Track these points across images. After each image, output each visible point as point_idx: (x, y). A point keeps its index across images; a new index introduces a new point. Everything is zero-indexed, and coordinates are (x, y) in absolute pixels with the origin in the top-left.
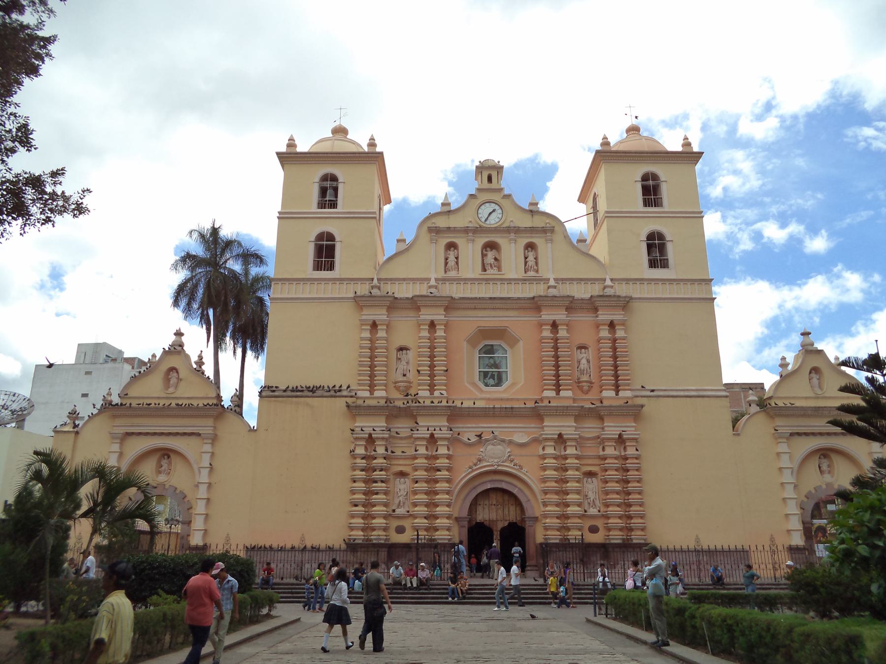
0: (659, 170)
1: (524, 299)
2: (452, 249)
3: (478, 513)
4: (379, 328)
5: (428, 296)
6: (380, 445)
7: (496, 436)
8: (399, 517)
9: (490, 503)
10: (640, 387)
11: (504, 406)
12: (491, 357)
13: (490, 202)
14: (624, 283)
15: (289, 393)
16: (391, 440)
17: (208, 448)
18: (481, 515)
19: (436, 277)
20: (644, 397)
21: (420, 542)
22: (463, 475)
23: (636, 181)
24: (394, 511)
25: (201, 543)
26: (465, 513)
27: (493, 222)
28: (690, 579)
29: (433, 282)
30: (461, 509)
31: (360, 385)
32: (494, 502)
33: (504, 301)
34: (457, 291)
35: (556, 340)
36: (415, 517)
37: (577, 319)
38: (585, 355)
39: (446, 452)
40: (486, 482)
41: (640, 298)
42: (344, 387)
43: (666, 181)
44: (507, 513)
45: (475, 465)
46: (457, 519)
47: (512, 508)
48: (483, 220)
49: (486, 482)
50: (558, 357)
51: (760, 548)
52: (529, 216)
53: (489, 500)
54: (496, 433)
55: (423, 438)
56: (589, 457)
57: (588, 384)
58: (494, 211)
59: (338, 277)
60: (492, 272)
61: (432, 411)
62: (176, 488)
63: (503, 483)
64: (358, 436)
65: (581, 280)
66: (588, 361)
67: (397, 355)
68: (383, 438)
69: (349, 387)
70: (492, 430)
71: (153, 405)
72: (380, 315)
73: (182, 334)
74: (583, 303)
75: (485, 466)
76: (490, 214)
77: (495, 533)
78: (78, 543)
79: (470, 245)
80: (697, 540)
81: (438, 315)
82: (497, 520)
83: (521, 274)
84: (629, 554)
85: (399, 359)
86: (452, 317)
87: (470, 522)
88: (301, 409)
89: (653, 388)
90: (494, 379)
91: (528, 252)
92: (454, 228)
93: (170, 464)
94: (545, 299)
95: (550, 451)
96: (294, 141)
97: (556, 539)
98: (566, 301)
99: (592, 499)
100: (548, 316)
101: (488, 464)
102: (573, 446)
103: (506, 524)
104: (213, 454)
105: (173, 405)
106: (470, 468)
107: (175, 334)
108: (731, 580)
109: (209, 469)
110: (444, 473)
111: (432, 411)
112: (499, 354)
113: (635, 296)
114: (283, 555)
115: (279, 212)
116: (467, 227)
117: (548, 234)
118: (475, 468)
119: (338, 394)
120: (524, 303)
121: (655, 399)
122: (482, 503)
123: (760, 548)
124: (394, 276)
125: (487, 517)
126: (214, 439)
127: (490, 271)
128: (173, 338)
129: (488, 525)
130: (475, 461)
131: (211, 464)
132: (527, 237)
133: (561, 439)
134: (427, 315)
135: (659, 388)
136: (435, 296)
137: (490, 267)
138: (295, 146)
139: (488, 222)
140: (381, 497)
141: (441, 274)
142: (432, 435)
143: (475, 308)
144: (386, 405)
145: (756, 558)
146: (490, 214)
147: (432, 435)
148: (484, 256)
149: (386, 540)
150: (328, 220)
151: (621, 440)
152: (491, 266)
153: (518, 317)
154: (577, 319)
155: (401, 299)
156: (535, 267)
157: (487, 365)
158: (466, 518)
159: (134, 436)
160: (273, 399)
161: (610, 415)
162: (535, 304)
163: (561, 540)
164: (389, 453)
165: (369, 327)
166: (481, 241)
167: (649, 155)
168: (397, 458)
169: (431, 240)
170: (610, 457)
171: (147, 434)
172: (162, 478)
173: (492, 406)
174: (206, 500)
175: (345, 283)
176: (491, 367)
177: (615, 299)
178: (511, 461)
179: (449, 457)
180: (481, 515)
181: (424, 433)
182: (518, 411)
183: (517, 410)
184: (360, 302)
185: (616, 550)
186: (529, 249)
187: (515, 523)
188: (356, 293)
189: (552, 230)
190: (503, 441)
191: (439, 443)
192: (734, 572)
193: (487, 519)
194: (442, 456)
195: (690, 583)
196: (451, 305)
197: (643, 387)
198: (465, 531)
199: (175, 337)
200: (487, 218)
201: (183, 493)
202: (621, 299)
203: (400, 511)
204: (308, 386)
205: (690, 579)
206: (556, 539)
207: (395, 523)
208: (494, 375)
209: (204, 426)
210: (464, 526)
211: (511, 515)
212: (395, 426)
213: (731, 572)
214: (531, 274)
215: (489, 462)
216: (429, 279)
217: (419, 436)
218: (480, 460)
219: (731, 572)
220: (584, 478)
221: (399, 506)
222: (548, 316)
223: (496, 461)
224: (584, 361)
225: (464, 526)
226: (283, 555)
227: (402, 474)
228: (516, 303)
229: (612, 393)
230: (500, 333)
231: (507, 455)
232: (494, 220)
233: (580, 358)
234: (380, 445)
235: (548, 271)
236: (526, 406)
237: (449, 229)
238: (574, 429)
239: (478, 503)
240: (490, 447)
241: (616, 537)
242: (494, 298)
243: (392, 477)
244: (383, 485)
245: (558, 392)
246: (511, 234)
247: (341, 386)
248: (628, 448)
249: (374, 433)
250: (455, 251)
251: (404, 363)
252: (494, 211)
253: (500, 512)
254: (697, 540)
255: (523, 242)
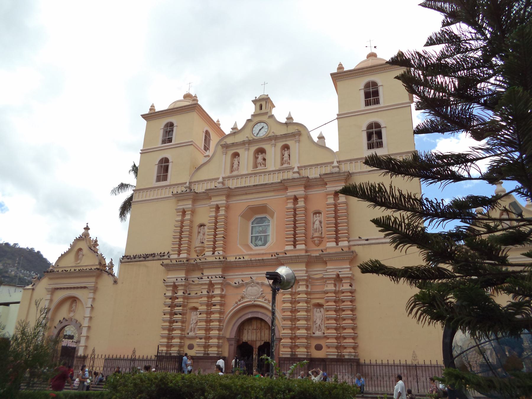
0: (376, 78)
1: (276, 183)
2: (237, 156)
3: (244, 335)
4: (220, 209)
5: (214, 189)
6: (217, 288)
7: (253, 280)
8: (318, 338)
9: (252, 328)
10: (358, 238)
11: (257, 259)
12: (260, 226)
13: (260, 122)
14: (348, 163)
15: (137, 259)
16: (189, 286)
17: (91, 295)
18: (246, 336)
19: (299, 165)
20: (360, 245)
21: (159, 354)
22: (231, 308)
23: (360, 90)
24: (188, 334)
25: (82, 355)
26: (233, 335)
27: (261, 135)
28: (388, 389)
29: (335, 164)
30: (230, 332)
31: (173, 251)
32: (255, 328)
33: (263, 187)
34: (233, 184)
35: (295, 210)
36: (327, 338)
37: (315, 192)
38: (318, 218)
39: (219, 292)
40: (248, 313)
41: (359, 172)
42: (166, 254)
43: (382, 85)
44: (263, 335)
45: (240, 301)
46: (229, 340)
47: (267, 332)
48: (255, 135)
49: (248, 313)
50: (217, 228)
51: (100, 357)
52: (285, 127)
53: (252, 326)
54: (254, 278)
55: (205, 284)
56: (318, 293)
57: (319, 239)
58: (263, 127)
59: (169, 184)
60: (260, 168)
61: (211, 265)
62: (77, 321)
63: (259, 313)
64: (167, 284)
65: (318, 165)
66: (320, 222)
67: (198, 230)
68: (182, 285)
69: (168, 253)
70: (250, 276)
71: (88, 270)
72: (188, 205)
73: (89, 229)
74: (316, 181)
75: (247, 301)
76: (260, 130)
77: (254, 350)
78: (93, 355)
79: (247, 152)
80: (415, 356)
81: (300, 192)
82: (256, 341)
83: (278, 167)
84: (341, 366)
85: (199, 232)
86: (232, 201)
87: (238, 341)
88: (140, 268)
89: (366, 238)
90: (261, 241)
91: (285, 151)
92: (236, 143)
93: (76, 306)
94: (288, 181)
95: (331, 287)
96: (197, 98)
97: (288, 354)
98: (303, 181)
99: (318, 324)
100: (291, 193)
101: (248, 300)
102: (303, 285)
103: (262, 343)
104: (94, 299)
105: (77, 270)
106: (236, 303)
107: (85, 229)
108: (374, 390)
109: (90, 308)
110: (302, 323)
111: (211, 265)
112: (265, 223)
113: (354, 171)
114: (141, 363)
115: (141, 150)
116: (244, 141)
117: (296, 137)
118: (239, 303)
119: (162, 258)
120: (275, 186)
121: (368, 246)
122: (247, 328)
123: (100, 357)
124: (198, 180)
125: (250, 338)
126: (95, 290)
127: (259, 167)
128: (83, 231)
129: (250, 344)
130: (239, 298)
131: (92, 306)
132: (283, 141)
133: (338, 279)
134: (215, 201)
135: (372, 238)
136: (218, 189)
137: (260, 165)
138: (343, 68)
139: (258, 136)
140: (179, 324)
141: (228, 174)
142: (211, 281)
143: (246, 194)
144: (224, 260)
145: (100, 362)
146: (260, 130)
147: (211, 281)
148: (256, 158)
149: (355, 356)
150: (166, 150)
151: (338, 279)
152: (261, 165)
153: (275, 196)
154: (315, 192)
155: (200, 193)
156: (289, 161)
157: (258, 232)
158: (233, 339)
159: (59, 290)
160: (127, 263)
161: (331, 260)
162: (283, 185)
163: (338, 355)
164: (187, 295)
165: (332, 196)
166: (253, 149)
167: (348, 73)
168: (192, 298)
169: (223, 152)
170: (331, 292)
171: (64, 288)
172: (72, 314)
173: (250, 259)
174: (87, 328)
175: (272, 174)
176: (260, 233)
177: (337, 175)
178: (263, 297)
179: (222, 296)
180: (246, 336)
181: (206, 280)
182: (268, 262)
183: (266, 261)
184: (179, 197)
185: (333, 363)
186: (286, 149)
187: (247, 342)
188: (172, 192)
189: (299, 134)
190: (258, 283)
191: (215, 287)
192: (379, 382)
193: (250, 340)
194: (217, 295)
195: (380, 393)
196: (230, 193)
197: (360, 238)
198: (233, 348)
199: (84, 230)
200: (258, 133)
201: (80, 324)
202: (342, 175)
203: (318, 333)
204: (147, 254)
205: (388, 389)
206: (288, 354)
207: (314, 343)
208: (262, 238)
209: (90, 282)
210: (232, 345)
211: (266, 336)
212: (193, 276)
213: (388, 383)
214: (285, 166)
215: (248, 299)
216: (333, 163)
217: (202, 282)
218: (243, 298)
219: (388, 383)
220: (313, 309)
221: (191, 331)
222: (291, 193)
223: (253, 297)
224: (317, 223)
225: (232, 345)
226: (141, 363)
227: (320, 306)
228: (272, 187)
229: (334, 244)
230: (263, 209)
231: (260, 293)
232: (262, 134)
233: (315, 220)
234: (217, 288)
235: (295, 164)
236: (324, 253)
237: (233, 145)
238: (348, 270)
239: (245, 328)
240: (250, 288)
241: (332, 353)
242: (257, 185)
243: (188, 310)
244: (180, 316)
245: (295, 246)
246: (273, 141)
247: (164, 253)
248: (344, 285)
249: (176, 282)
250: (239, 158)
251: (201, 234)
252: (263, 127)
253: (259, 334)
254: (415, 356)
255: (280, 144)
